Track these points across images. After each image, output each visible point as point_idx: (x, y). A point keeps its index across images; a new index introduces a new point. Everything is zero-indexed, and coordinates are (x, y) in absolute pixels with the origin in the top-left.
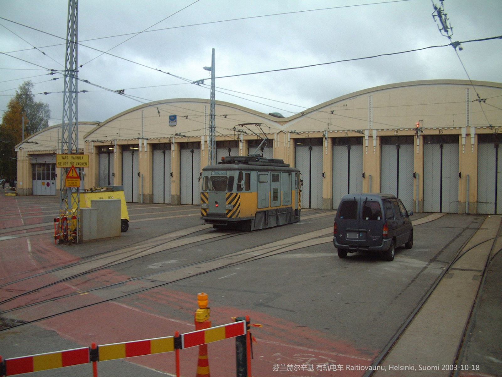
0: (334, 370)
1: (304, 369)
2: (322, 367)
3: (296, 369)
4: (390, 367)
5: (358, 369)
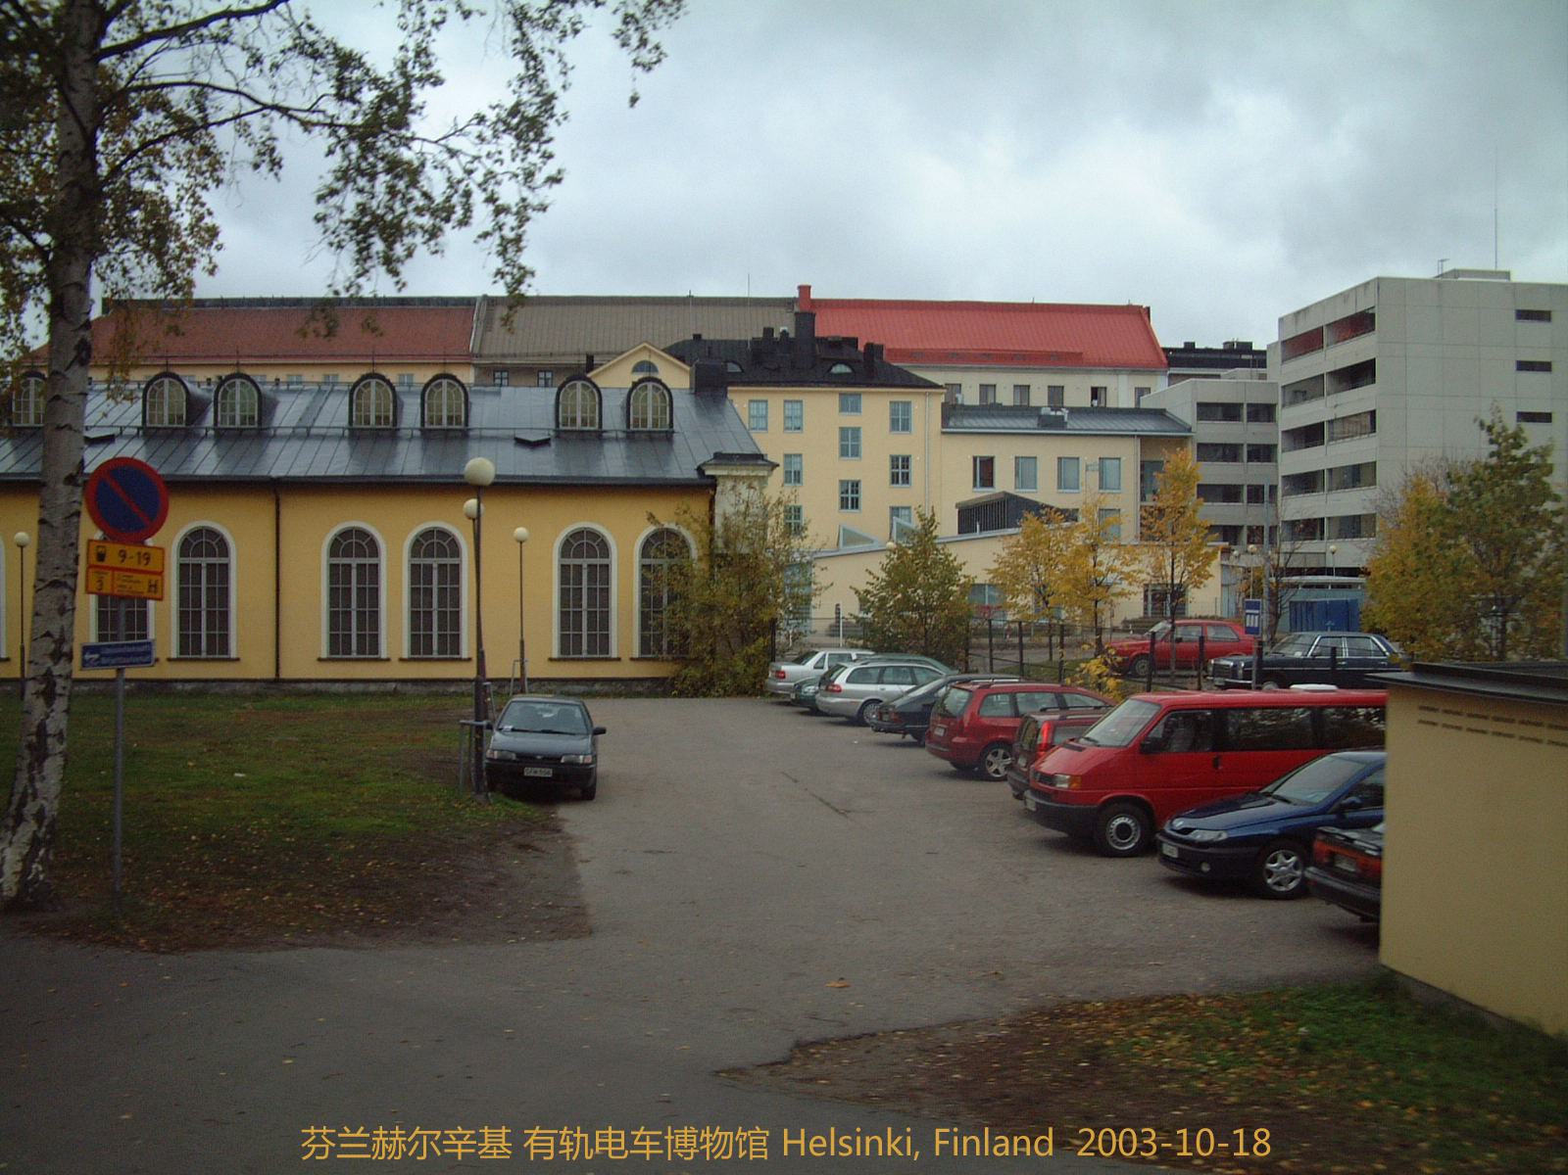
0: (615, 1153)
1: (460, 1151)
2: (552, 1138)
3: (419, 1151)
4: (786, 1142)
5: (1022, 1143)
